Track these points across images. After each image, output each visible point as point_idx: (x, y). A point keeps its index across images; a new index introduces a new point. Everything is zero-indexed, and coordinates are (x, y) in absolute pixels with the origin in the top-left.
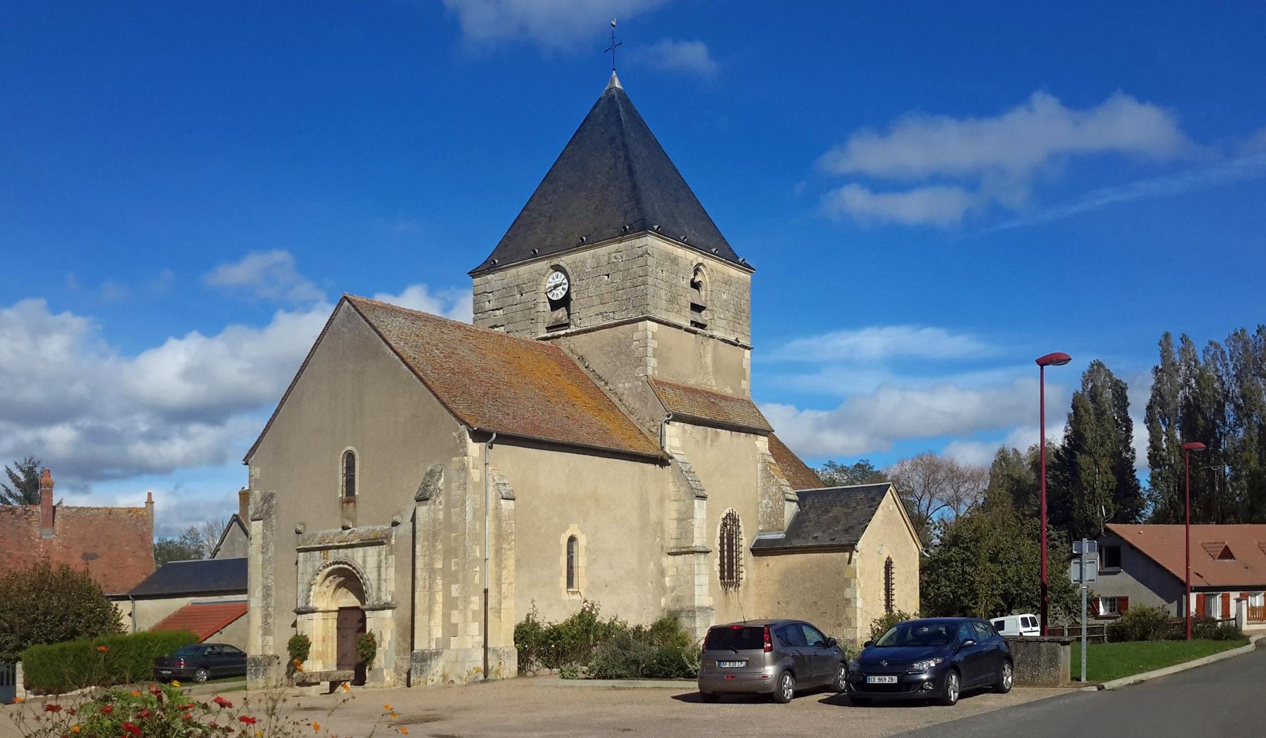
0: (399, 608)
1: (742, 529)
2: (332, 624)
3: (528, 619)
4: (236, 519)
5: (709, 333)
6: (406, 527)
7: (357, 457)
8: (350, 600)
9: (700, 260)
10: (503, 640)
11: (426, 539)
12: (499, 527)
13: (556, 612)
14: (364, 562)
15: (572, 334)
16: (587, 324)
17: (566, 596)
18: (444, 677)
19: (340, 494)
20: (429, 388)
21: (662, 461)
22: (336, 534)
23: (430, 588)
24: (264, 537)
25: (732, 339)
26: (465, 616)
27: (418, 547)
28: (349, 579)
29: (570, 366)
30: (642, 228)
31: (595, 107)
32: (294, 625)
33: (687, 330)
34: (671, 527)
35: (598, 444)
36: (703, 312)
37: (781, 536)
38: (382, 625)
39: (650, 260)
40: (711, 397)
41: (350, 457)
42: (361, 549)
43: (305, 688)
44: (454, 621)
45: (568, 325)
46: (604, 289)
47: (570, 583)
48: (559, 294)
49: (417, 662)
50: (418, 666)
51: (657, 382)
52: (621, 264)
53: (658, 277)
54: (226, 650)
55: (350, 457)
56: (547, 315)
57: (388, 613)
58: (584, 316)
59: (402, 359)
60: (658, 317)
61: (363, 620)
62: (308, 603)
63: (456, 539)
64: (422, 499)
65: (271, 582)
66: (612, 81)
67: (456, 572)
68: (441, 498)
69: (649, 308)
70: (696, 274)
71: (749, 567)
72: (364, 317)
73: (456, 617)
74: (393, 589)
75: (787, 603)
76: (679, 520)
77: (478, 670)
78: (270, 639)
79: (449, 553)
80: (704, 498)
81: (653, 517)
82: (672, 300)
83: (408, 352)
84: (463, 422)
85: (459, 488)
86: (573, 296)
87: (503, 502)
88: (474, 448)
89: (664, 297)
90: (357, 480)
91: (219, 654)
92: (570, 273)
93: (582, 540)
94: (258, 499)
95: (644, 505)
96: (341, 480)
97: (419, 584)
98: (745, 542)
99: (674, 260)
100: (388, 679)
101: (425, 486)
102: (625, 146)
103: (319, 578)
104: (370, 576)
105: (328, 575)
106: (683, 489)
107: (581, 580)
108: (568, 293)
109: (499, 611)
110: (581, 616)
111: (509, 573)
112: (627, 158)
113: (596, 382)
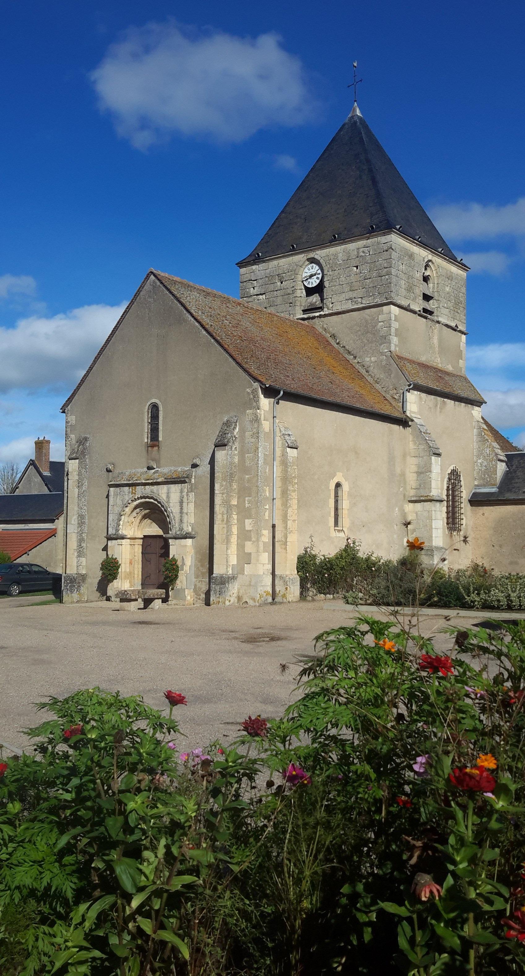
0: (198, 538)
1: (462, 483)
2: (138, 549)
3: (306, 551)
4: (32, 463)
5: (435, 318)
6: (205, 468)
7: (161, 408)
8: (154, 530)
9: (430, 257)
10: (288, 568)
11: (224, 479)
12: (285, 471)
13: (327, 549)
14: (168, 497)
15: (325, 316)
16: (338, 308)
17: (333, 534)
18: (239, 598)
19: (146, 439)
20: (225, 350)
21: (403, 422)
22: (142, 473)
23: (228, 521)
24: (80, 474)
25: (453, 324)
26: (258, 546)
27: (217, 486)
28: (154, 511)
29: (323, 342)
30: (387, 227)
31: (340, 130)
32: (105, 549)
33: (420, 315)
34: (412, 479)
35: (358, 405)
36: (431, 302)
37: (494, 490)
38: (184, 552)
39: (394, 255)
40: (440, 373)
41: (155, 408)
42: (165, 487)
43: (125, 604)
44: (247, 550)
45: (321, 309)
46: (353, 278)
47: (336, 523)
48: (314, 282)
49: (213, 584)
50: (218, 588)
51: (400, 358)
52: (368, 258)
53: (399, 268)
54: (35, 569)
55: (155, 408)
56: (303, 300)
57: (189, 542)
58: (335, 301)
59: (202, 326)
60: (399, 302)
61: (166, 547)
62: (117, 530)
63: (249, 480)
64: (220, 444)
65: (84, 512)
66: (354, 110)
67: (249, 509)
68: (237, 444)
69: (393, 295)
70: (426, 269)
71: (469, 516)
72: (168, 290)
73: (249, 547)
74: (193, 522)
75: (501, 546)
76: (419, 473)
77: (268, 594)
78: (83, 560)
79: (244, 492)
80: (439, 455)
81: (398, 470)
82: (410, 289)
83: (206, 320)
84: (256, 379)
85: (252, 436)
86: (326, 284)
87: (288, 449)
88: (265, 403)
89: (403, 286)
90: (161, 428)
91: (29, 572)
92: (324, 264)
93: (346, 487)
94: (74, 442)
95: (391, 459)
96: (146, 428)
97: (218, 518)
98: (465, 494)
99: (411, 256)
100: (189, 598)
101: (223, 434)
102: (368, 161)
103: (128, 510)
104: (173, 509)
105: (135, 508)
106: (422, 447)
107: (345, 521)
108: (322, 282)
109: (285, 543)
110: (345, 550)
111: (292, 512)
112: (370, 170)
113: (346, 356)
